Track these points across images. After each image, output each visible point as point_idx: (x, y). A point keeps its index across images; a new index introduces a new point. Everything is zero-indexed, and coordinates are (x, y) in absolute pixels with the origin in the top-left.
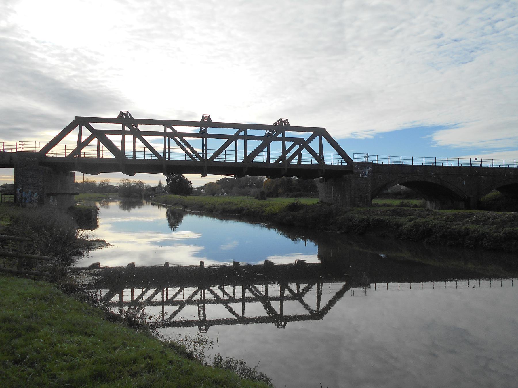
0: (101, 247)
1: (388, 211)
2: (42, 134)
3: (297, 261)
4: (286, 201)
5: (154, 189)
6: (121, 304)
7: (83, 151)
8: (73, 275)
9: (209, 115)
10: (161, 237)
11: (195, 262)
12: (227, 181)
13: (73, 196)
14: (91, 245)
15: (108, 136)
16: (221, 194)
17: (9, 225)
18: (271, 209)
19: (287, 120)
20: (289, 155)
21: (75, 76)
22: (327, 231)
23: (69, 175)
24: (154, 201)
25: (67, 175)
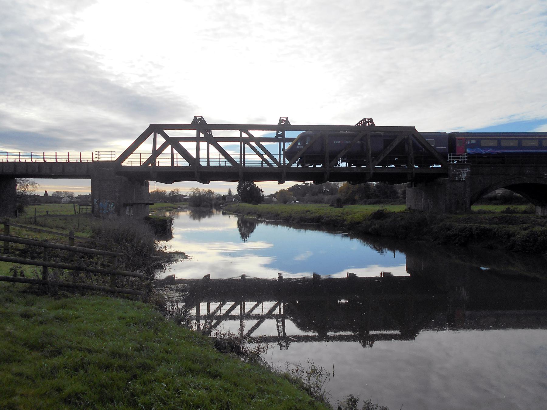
0: (181, 260)
1: (495, 219)
2: (112, 144)
3: (382, 273)
4: (370, 209)
5: (224, 197)
6: (198, 317)
7: (157, 160)
8: (159, 290)
9: (287, 118)
10: (232, 247)
11: (272, 275)
12: (299, 188)
13: (148, 206)
14: (171, 258)
15: (181, 143)
16: (293, 202)
17: (91, 237)
18: (353, 218)
19: (371, 119)
20: (282, 163)
21: (142, 83)
22: (421, 242)
23: (144, 185)
24: (226, 210)
25: (142, 184)
